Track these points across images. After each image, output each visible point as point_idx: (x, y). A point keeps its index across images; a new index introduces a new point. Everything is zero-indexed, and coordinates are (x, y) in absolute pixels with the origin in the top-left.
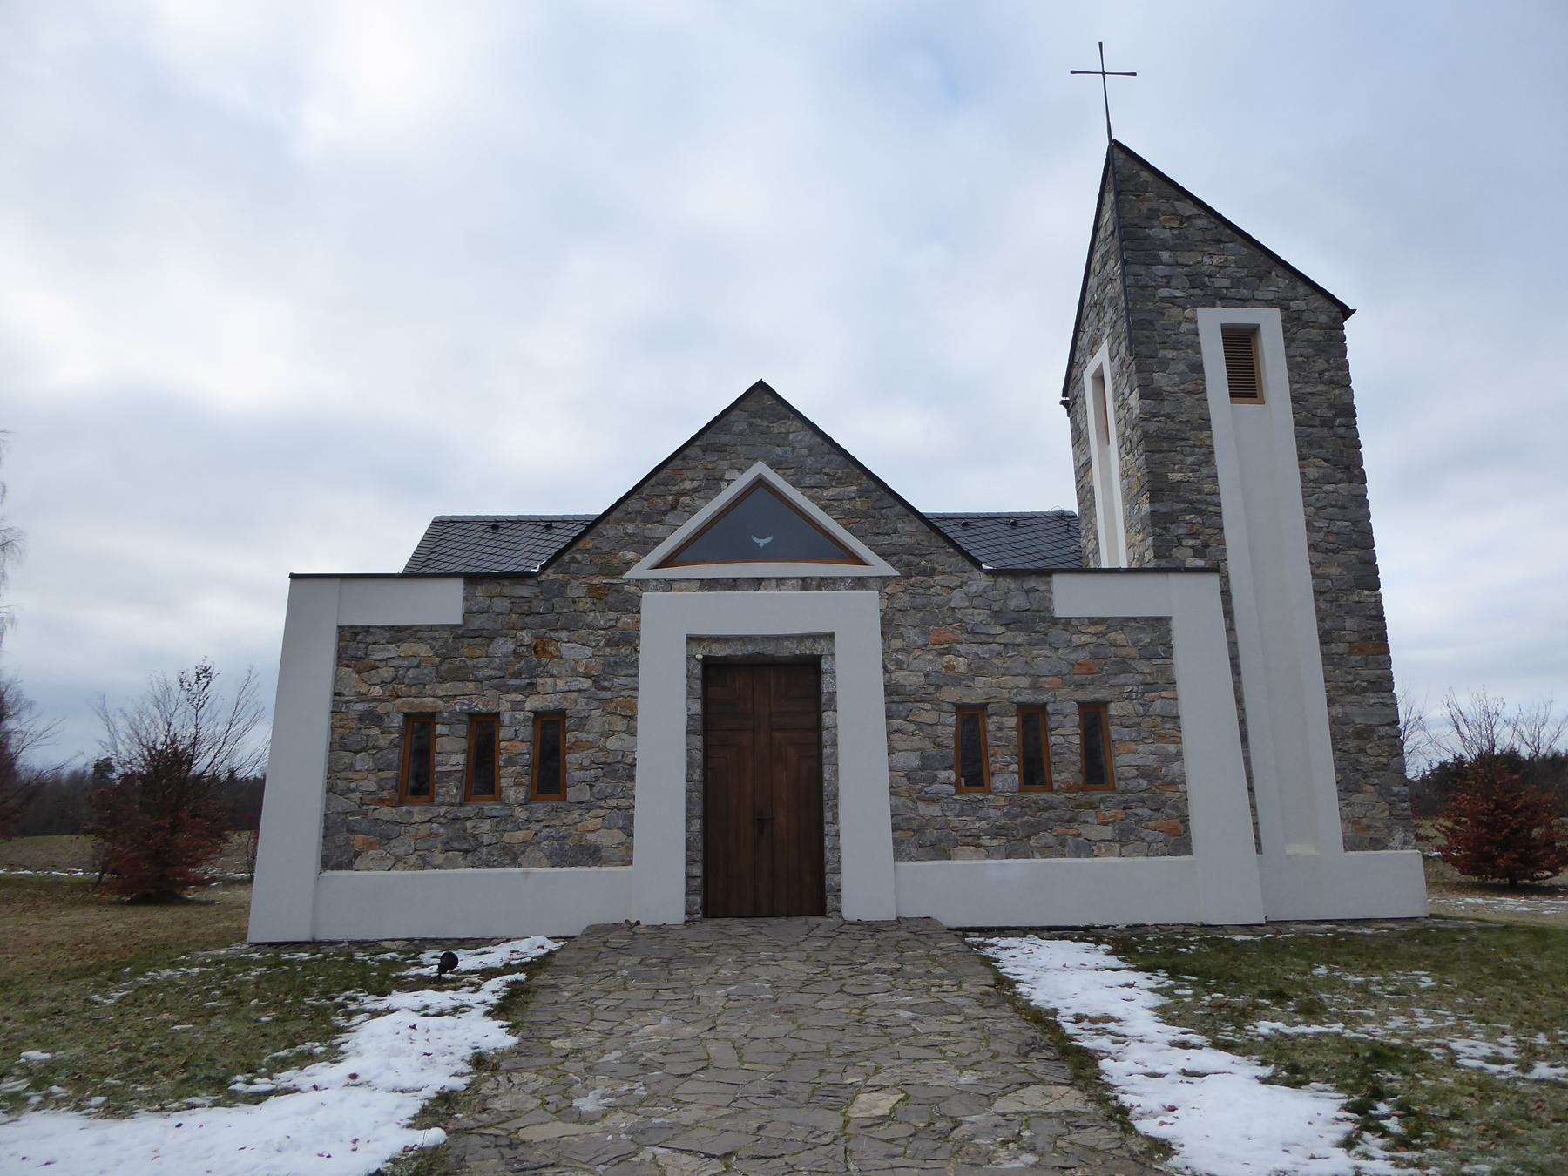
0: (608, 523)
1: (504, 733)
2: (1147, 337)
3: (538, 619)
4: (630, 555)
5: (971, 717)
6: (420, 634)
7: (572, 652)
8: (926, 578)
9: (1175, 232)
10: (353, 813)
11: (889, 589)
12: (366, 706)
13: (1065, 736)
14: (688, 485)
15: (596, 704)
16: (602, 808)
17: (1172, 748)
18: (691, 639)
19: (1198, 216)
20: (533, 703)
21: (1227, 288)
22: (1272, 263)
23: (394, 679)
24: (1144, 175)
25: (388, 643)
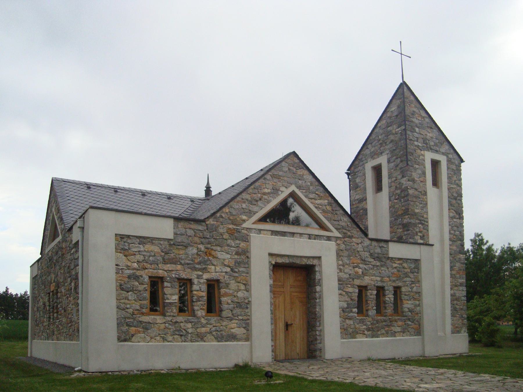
0: (234, 202)
1: (195, 287)
2: (411, 159)
3: (207, 240)
4: (244, 217)
5: (362, 289)
6: (154, 241)
7: (222, 256)
8: (350, 239)
9: (420, 122)
10: (129, 318)
11: (338, 242)
12: (131, 272)
13: (389, 297)
14: (266, 191)
15: (232, 278)
16: (236, 319)
17: (417, 302)
18: (271, 255)
19: (426, 117)
20: (206, 276)
21: (433, 146)
22: (444, 140)
23: (143, 261)
24: (412, 98)
25: (139, 244)
